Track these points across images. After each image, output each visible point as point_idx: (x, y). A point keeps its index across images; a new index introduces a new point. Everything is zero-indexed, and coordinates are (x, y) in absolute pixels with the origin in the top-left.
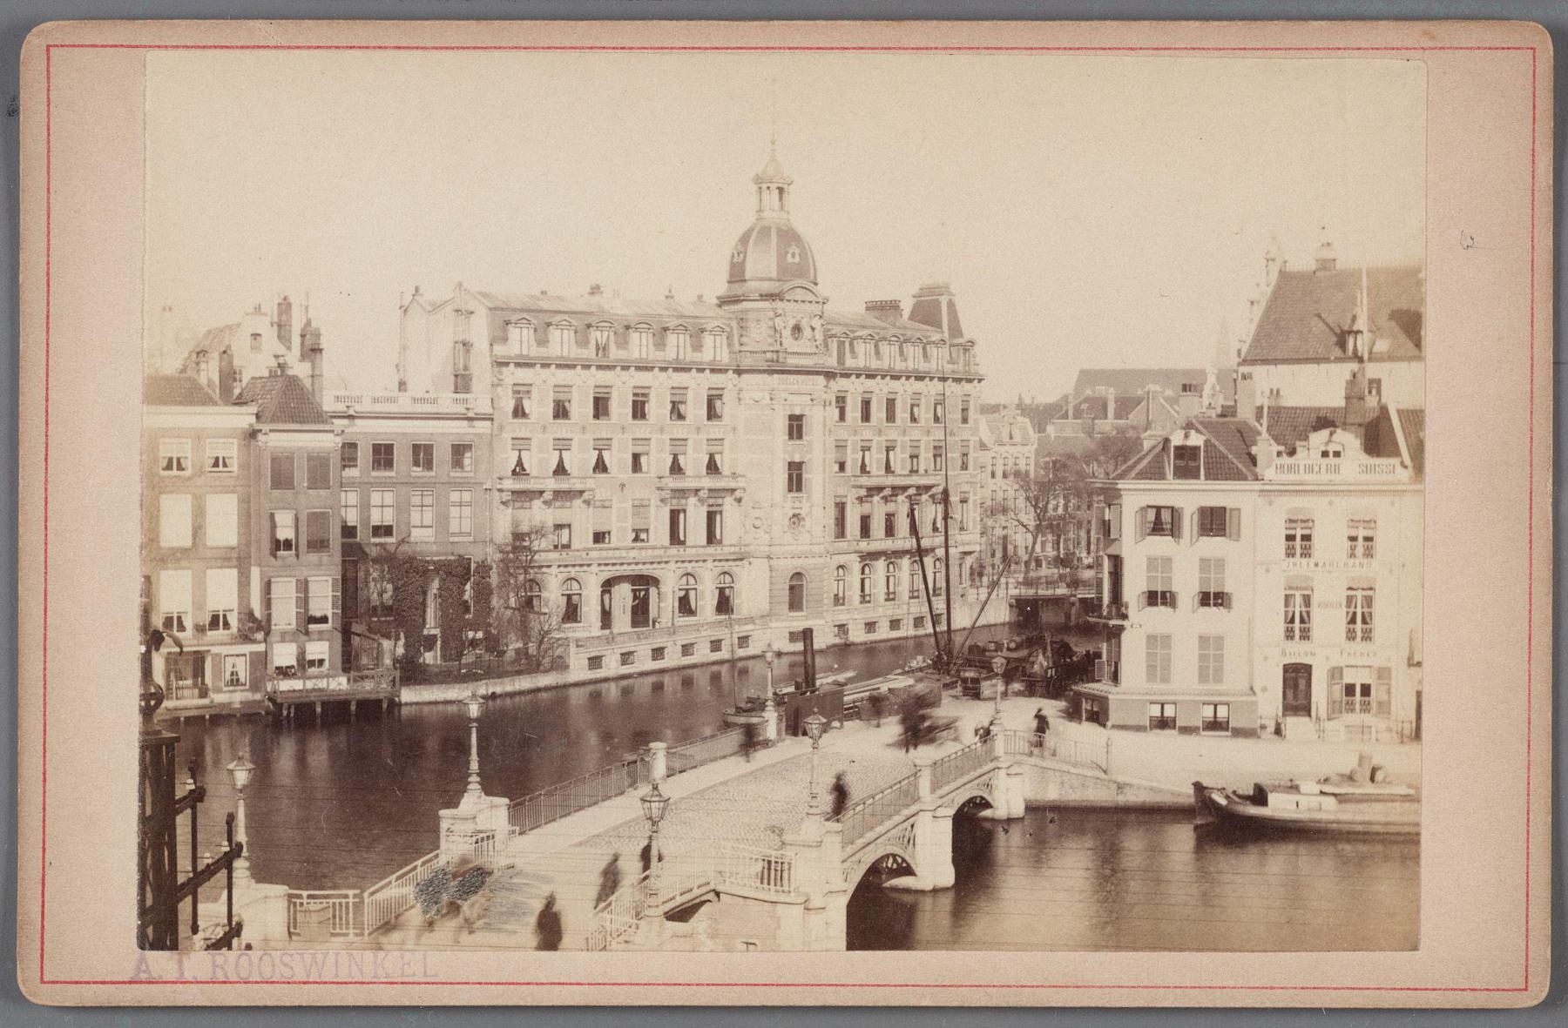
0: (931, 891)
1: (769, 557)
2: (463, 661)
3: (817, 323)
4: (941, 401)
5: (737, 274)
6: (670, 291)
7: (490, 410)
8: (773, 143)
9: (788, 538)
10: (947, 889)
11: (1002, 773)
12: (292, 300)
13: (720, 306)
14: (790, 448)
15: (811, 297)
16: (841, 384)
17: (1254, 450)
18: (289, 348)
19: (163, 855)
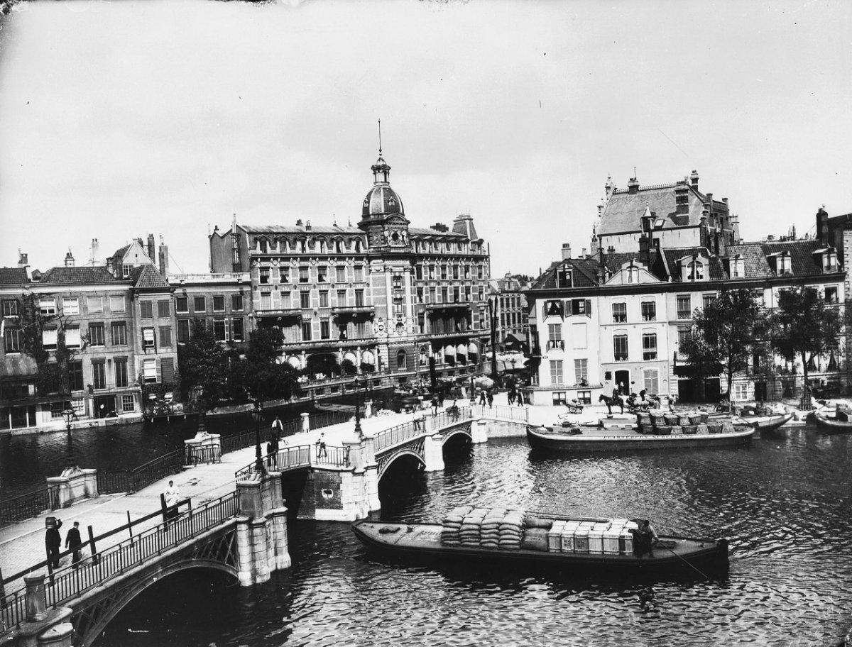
1: (387, 344)
3: (404, 233)
7: (249, 280)
18: (154, 262)
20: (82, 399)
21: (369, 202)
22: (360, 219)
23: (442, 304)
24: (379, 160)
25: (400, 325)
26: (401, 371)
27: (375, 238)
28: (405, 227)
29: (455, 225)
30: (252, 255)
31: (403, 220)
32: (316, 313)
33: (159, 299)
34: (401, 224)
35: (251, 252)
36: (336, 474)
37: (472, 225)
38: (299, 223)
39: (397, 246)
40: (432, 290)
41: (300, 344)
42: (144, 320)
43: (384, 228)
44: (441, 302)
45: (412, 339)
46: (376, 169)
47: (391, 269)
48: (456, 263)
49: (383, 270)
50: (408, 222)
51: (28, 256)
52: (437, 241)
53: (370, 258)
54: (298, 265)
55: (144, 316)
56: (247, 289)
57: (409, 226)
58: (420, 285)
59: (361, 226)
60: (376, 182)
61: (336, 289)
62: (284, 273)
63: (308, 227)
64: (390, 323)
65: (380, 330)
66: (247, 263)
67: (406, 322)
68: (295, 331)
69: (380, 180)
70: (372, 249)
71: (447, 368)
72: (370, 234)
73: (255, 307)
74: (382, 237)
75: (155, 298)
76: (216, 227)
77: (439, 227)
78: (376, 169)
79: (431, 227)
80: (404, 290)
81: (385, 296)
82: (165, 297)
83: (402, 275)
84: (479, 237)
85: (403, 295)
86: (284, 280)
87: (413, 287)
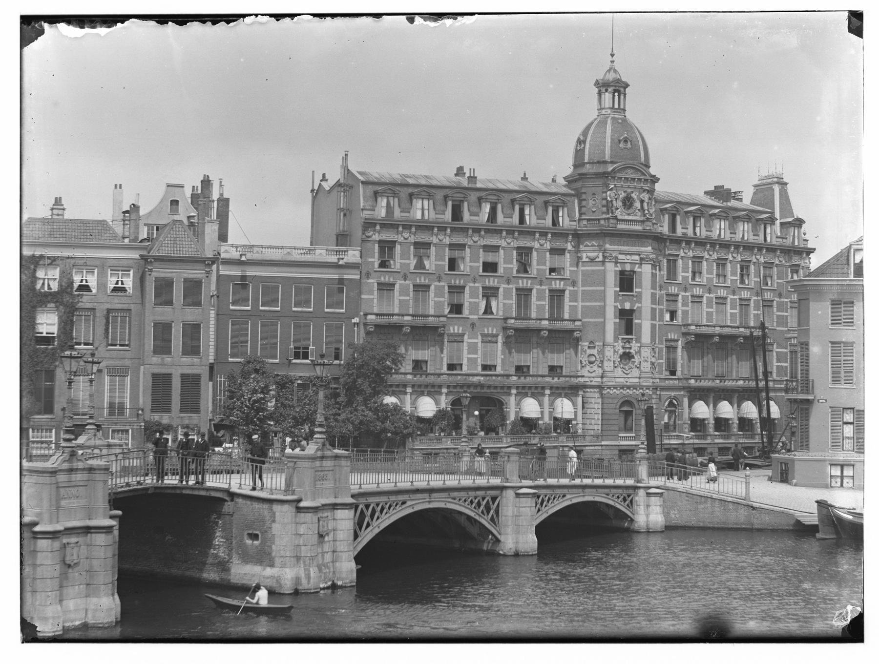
2: (338, 400)
6: (525, 174)
8: (612, 55)
9: (619, 372)
10: (532, 555)
11: (510, 494)
14: (620, 298)
15: (638, 176)
19: (596, 301)
20: (51, 431)
21: (584, 142)
22: (568, 170)
23: (738, 327)
24: (609, 71)
25: (627, 356)
26: (625, 438)
27: (591, 202)
28: (647, 187)
29: (755, 193)
30: (366, 219)
31: (643, 174)
32: (473, 325)
33: (185, 275)
34: (640, 180)
35: (366, 214)
37: (784, 196)
38: (460, 171)
39: (630, 218)
41: (439, 375)
42: (160, 309)
43: (607, 186)
44: (738, 324)
45: (649, 383)
46: (602, 86)
47: (616, 258)
48: (698, 253)
49: (601, 259)
50: (654, 180)
52: (711, 215)
53: (578, 237)
54: (447, 241)
55: (158, 302)
56: (353, 275)
57: (657, 186)
59: (570, 181)
60: (601, 109)
62: (456, 254)
63: (473, 179)
64: (609, 352)
65: (591, 363)
66: (358, 233)
67: (639, 352)
68: (535, 355)
69: (607, 106)
70: (585, 222)
71: (717, 441)
72: (584, 196)
73: (364, 308)
74: (604, 202)
75: (179, 275)
76: (324, 175)
77: (720, 193)
78: (602, 86)
79: (706, 193)
80: (639, 296)
81: (603, 304)
82: (196, 273)
83: (637, 269)
85: (637, 305)
87: (658, 292)
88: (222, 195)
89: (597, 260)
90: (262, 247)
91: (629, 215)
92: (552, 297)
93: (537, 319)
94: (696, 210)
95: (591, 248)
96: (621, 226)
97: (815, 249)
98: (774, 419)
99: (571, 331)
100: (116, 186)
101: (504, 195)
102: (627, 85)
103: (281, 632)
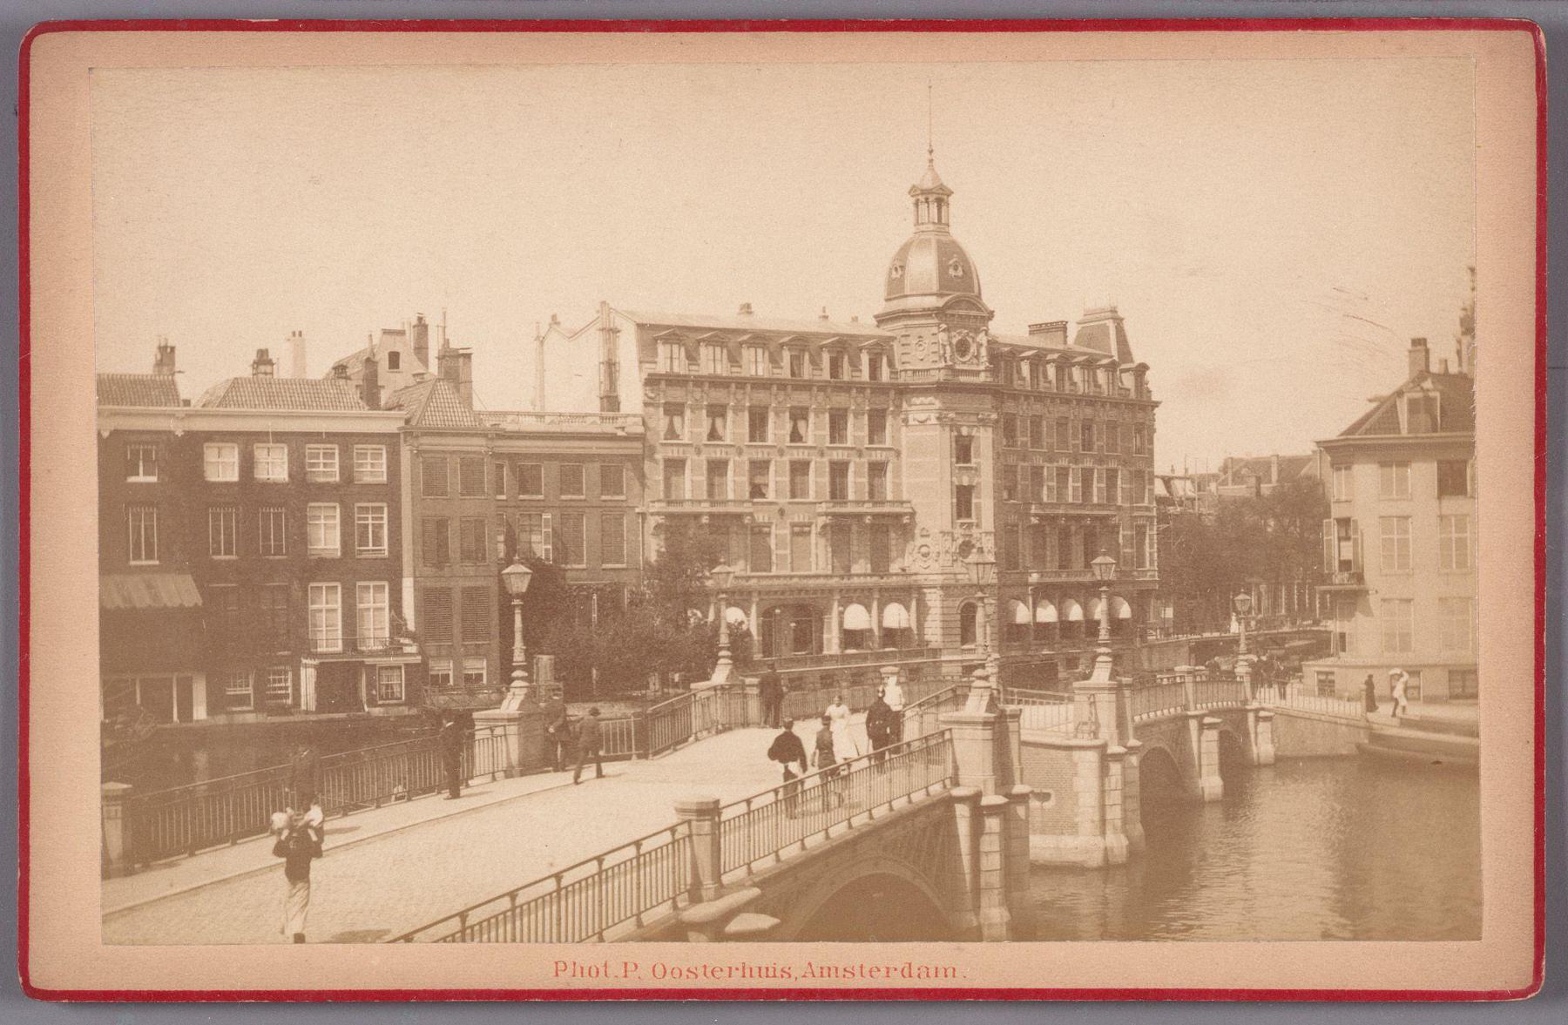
0: (1099, 869)
4: (1062, 423)
5: (895, 288)
7: (640, 429)
8: (931, 152)
12: (428, 321)
13: (878, 326)
16: (1010, 407)
17: (246, 371)
36: (1063, 753)
40: (1063, 474)
51: (177, 352)
58: (1012, 460)
61: (786, 458)
76: (554, 317)
84: (1138, 359)
86: (796, 436)
88: (447, 342)
89: (929, 422)
90: (518, 414)
91: (964, 363)
92: (833, 470)
93: (692, 501)
94: (711, 336)
95: (921, 407)
96: (963, 379)
97: (1160, 403)
98: (1123, 620)
99: (898, 516)
100: (294, 334)
101: (687, 334)
102: (950, 193)
103: (431, 931)
